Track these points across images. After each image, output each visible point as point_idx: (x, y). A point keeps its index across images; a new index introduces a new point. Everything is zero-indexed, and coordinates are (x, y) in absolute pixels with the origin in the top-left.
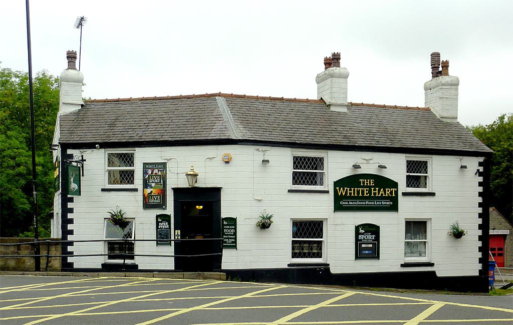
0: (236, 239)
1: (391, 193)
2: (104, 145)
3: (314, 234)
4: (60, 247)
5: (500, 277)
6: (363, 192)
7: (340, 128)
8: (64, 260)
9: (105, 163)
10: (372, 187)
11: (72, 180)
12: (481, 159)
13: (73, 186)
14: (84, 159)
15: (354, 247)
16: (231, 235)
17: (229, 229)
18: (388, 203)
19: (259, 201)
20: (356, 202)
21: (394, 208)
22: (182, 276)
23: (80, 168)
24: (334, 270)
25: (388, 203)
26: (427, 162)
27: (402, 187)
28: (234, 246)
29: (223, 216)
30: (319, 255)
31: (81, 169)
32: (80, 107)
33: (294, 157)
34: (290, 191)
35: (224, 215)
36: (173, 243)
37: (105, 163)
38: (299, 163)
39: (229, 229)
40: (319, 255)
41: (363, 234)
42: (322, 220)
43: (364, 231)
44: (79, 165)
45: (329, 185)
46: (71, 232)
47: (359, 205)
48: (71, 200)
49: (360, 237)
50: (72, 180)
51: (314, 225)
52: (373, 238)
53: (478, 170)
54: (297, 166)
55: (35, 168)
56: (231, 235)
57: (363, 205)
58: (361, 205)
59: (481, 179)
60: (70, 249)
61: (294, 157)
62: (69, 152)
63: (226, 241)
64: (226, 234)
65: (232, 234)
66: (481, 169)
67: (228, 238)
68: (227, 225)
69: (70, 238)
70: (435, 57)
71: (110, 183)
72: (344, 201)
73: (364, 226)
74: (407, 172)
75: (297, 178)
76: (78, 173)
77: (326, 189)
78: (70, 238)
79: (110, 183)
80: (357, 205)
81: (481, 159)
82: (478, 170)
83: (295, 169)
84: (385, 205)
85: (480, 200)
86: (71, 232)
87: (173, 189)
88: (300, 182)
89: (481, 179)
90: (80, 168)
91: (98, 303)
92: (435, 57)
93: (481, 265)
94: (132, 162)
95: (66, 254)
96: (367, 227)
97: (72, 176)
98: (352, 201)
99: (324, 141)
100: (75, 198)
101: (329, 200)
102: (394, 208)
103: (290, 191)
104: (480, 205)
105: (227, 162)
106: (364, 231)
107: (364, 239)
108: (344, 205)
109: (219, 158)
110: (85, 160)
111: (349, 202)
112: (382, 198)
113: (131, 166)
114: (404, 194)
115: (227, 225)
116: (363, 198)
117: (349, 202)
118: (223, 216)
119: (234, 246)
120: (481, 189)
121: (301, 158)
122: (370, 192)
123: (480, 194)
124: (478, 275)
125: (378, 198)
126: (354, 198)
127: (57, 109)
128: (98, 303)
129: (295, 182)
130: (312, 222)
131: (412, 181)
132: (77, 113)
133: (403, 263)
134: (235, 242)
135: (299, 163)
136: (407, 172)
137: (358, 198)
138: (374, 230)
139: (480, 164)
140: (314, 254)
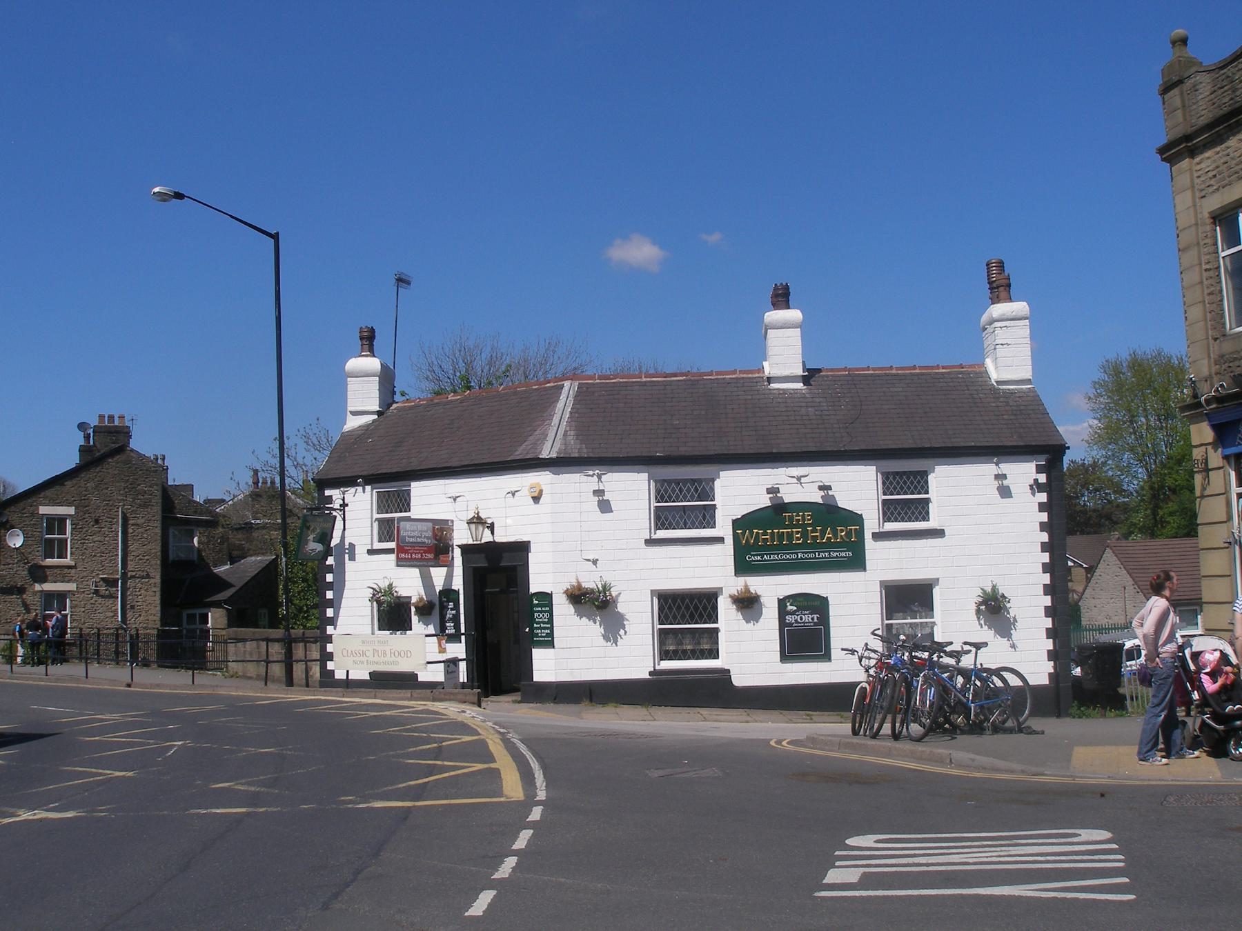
0: (552, 629)
1: (849, 533)
2: (371, 480)
3: (701, 616)
6: (790, 535)
9: (372, 506)
10: (809, 525)
14: (346, 502)
15: (778, 638)
16: (544, 623)
17: (541, 612)
18: (843, 554)
19: (595, 562)
20: (778, 554)
21: (857, 562)
22: (341, 694)
24: (740, 680)
25: (843, 554)
27: (872, 523)
28: (549, 643)
29: (533, 590)
30: (714, 654)
34: (650, 542)
35: (533, 589)
36: (463, 638)
37: (372, 506)
39: (541, 612)
40: (714, 654)
41: (793, 613)
43: (795, 608)
45: (723, 528)
47: (784, 560)
49: (789, 619)
51: (692, 599)
52: (816, 620)
53: (1036, 480)
55: (285, 521)
56: (544, 623)
57: (810, 558)
58: (788, 559)
59: (1043, 497)
63: (538, 634)
64: (537, 620)
65: (546, 620)
66: (1042, 478)
67: (540, 628)
68: (537, 605)
72: (754, 555)
73: (794, 598)
75: (662, 519)
80: (780, 560)
82: (1036, 480)
84: (837, 557)
85: (1045, 537)
89: (1043, 497)
91: (453, 737)
93: (1052, 663)
96: (802, 599)
98: (770, 555)
101: (726, 553)
102: (857, 562)
104: (1045, 547)
106: (795, 608)
107: (796, 621)
108: (844, 551)
110: (347, 505)
111: (797, 554)
112: (829, 545)
114: (877, 536)
115: (537, 605)
116: (791, 547)
117: (797, 554)
118: (533, 590)
119: (549, 643)
120: (1044, 517)
122: (805, 534)
123: (1043, 527)
124: (1048, 683)
125: (822, 545)
126: (766, 548)
128: (453, 737)
130: (687, 595)
131: (891, 510)
134: (551, 635)
137: (781, 547)
138: (817, 605)
139: (1039, 469)
140: (684, 652)
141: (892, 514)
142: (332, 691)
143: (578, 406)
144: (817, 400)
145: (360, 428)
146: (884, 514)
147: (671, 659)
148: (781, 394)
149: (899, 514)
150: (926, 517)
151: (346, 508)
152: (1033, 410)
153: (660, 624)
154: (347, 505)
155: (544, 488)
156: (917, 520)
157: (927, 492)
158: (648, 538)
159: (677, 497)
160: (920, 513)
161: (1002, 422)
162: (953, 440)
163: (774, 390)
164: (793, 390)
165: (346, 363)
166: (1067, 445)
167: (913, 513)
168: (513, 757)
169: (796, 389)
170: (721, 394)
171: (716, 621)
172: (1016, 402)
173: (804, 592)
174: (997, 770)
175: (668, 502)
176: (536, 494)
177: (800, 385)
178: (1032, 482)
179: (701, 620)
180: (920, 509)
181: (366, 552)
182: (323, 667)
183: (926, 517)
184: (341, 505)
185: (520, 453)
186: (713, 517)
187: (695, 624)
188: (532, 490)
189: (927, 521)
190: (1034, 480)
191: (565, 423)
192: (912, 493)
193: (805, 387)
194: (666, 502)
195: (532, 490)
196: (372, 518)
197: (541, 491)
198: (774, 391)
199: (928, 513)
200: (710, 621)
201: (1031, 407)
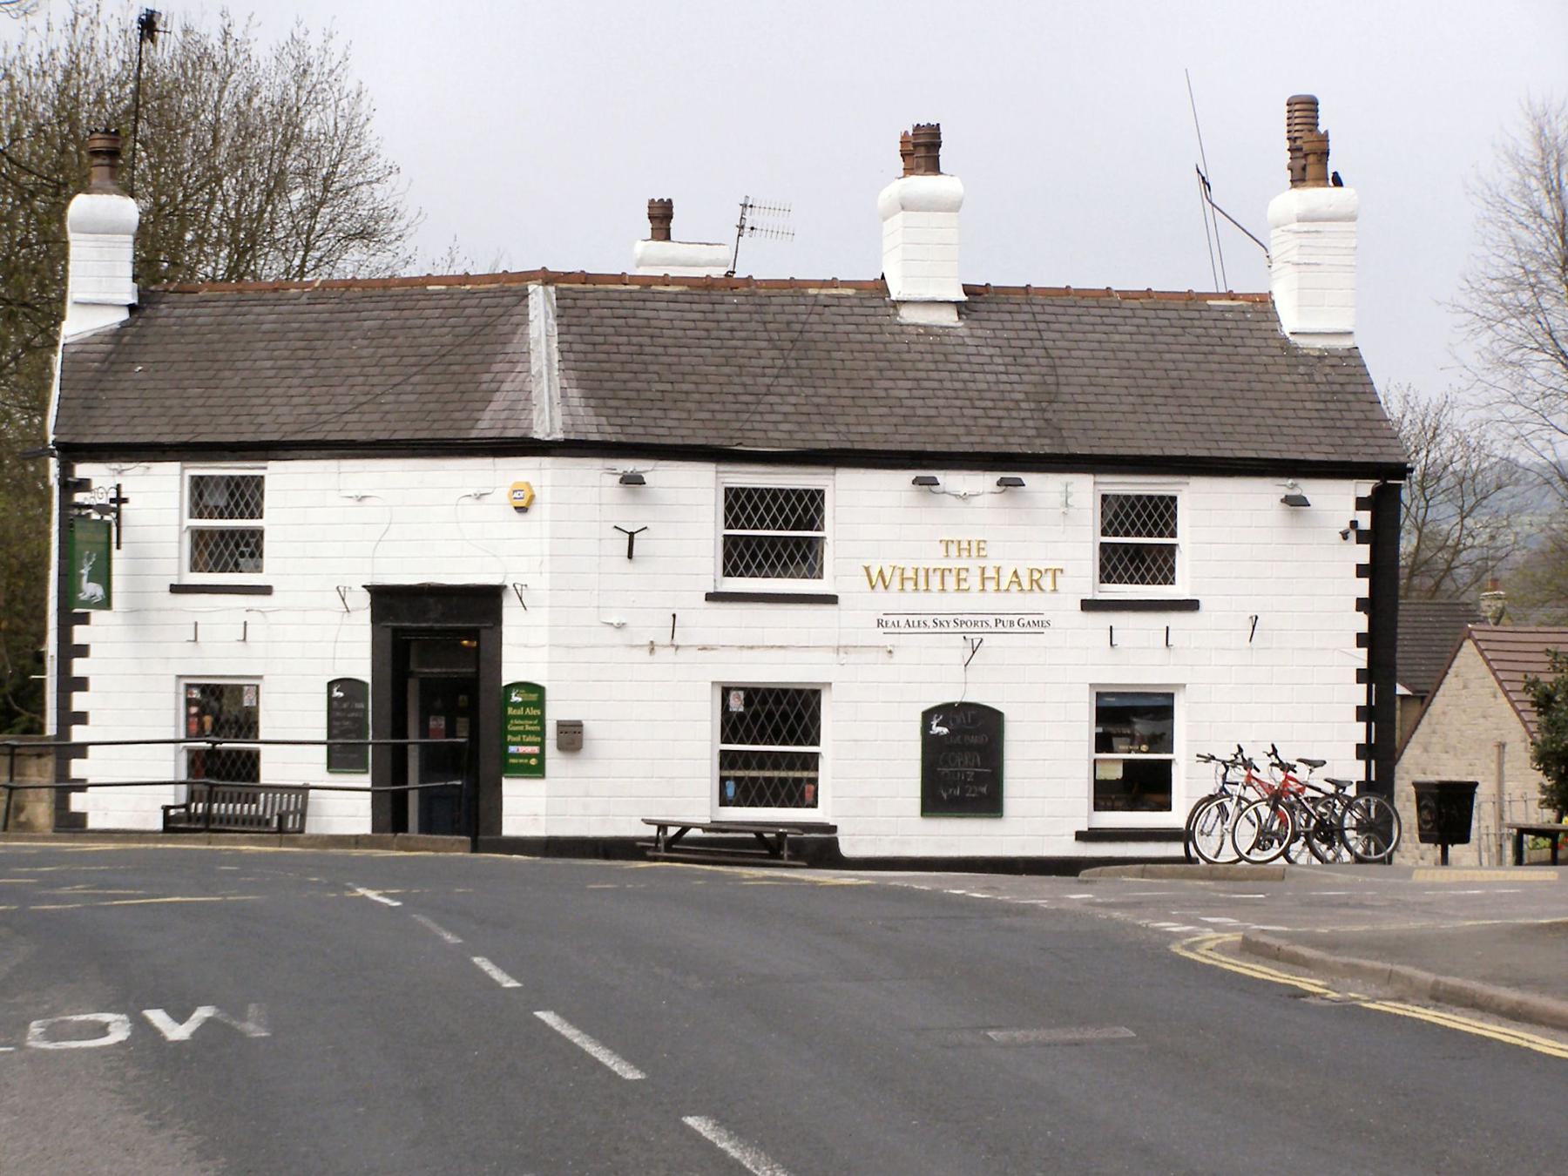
4: (49, 763)
5: (1561, 855)
7: (901, 390)
8: (61, 802)
11: (85, 571)
12: (1365, 488)
13: (91, 589)
19: (621, 626)
23: (109, 524)
26: (1174, 499)
29: (508, 678)
31: (114, 529)
32: (124, 315)
33: (728, 490)
34: (712, 597)
38: (743, 508)
42: (818, 688)
44: (107, 518)
46: (82, 718)
48: (84, 619)
50: (85, 571)
53: (1354, 524)
54: (736, 519)
60: (78, 768)
61: (728, 490)
62: (82, 470)
69: (78, 734)
70: (1304, 110)
71: (195, 567)
74: (1104, 533)
75: (738, 557)
76: (103, 537)
77: (9, 828)
78: (78, 734)
79: (195, 567)
81: (1365, 488)
82: (1354, 524)
83: (730, 527)
86: (82, 718)
87: (963, 285)
88: (747, 567)
90: (109, 524)
92: (1304, 110)
94: (259, 505)
95: (67, 786)
97: (89, 559)
99: (826, 439)
100: (96, 616)
103: (712, 597)
105: (521, 510)
109: (501, 499)
110: (125, 501)
113: (252, 516)
118: (508, 678)
121: (750, 493)
127: (60, 317)
129: (732, 567)
132: (117, 335)
133: (1477, 790)
135: (743, 508)
136: (1104, 533)
139: (1361, 504)
141: (1115, 569)
142: (179, 838)
143: (568, 338)
144: (985, 351)
145: (97, 339)
146: (1102, 568)
147: (783, 805)
148: (921, 334)
149: (1126, 569)
150: (1168, 577)
151: (123, 506)
152: (1355, 393)
153: (723, 743)
154: (125, 501)
155: (536, 491)
156: (1154, 581)
157: (1173, 535)
158: (712, 590)
159: (762, 520)
160: (1160, 570)
161: (1302, 414)
162: (1222, 445)
163: (908, 325)
164: (941, 327)
165: (65, 207)
166: (1409, 465)
167: (1148, 569)
168: (1447, 853)
169: (947, 327)
170: (816, 327)
171: (816, 742)
172: (1326, 375)
173: (535, 682)
174: (1276, 976)
175: (745, 528)
176: (522, 503)
177: (948, 317)
178: (1347, 525)
179: (748, 738)
180: (1159, 564)
181: (168, 588)
182: (61, 802)
183: (1168, 577)
184: (112, 500)
185: (486, 426)
186: (819, 557)
187: (739, 743)
188: (516, 495)
189: (1171, 583)
190: (1352, 522)
191: (557, 373)
192: (1150, 535)
193: (961, 324)
194: (743, 528)
195: (516, 495)
196: (181, 525)
197: (532, 497)
198: (910, 328)
199: (1172, 570)
200: (735, 739)
201: (1350, 388)
